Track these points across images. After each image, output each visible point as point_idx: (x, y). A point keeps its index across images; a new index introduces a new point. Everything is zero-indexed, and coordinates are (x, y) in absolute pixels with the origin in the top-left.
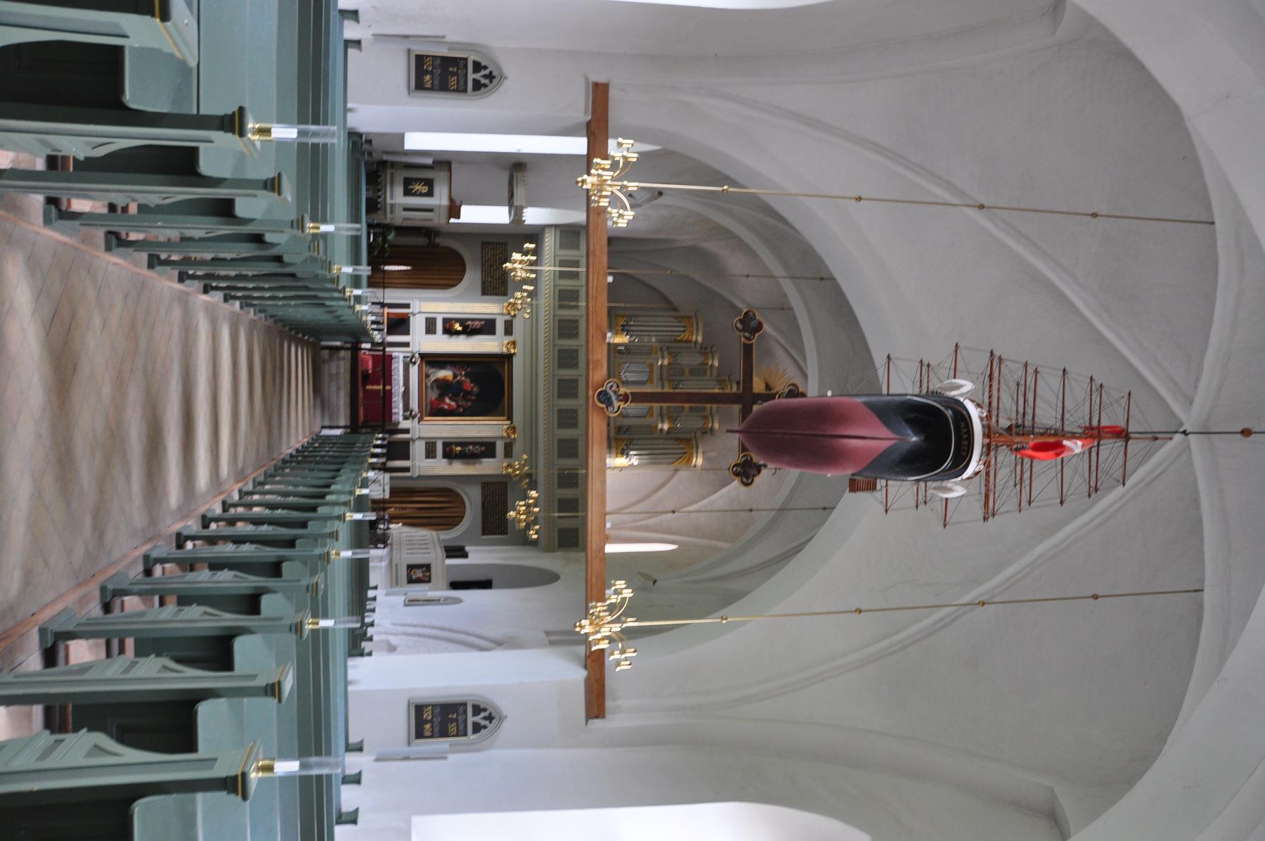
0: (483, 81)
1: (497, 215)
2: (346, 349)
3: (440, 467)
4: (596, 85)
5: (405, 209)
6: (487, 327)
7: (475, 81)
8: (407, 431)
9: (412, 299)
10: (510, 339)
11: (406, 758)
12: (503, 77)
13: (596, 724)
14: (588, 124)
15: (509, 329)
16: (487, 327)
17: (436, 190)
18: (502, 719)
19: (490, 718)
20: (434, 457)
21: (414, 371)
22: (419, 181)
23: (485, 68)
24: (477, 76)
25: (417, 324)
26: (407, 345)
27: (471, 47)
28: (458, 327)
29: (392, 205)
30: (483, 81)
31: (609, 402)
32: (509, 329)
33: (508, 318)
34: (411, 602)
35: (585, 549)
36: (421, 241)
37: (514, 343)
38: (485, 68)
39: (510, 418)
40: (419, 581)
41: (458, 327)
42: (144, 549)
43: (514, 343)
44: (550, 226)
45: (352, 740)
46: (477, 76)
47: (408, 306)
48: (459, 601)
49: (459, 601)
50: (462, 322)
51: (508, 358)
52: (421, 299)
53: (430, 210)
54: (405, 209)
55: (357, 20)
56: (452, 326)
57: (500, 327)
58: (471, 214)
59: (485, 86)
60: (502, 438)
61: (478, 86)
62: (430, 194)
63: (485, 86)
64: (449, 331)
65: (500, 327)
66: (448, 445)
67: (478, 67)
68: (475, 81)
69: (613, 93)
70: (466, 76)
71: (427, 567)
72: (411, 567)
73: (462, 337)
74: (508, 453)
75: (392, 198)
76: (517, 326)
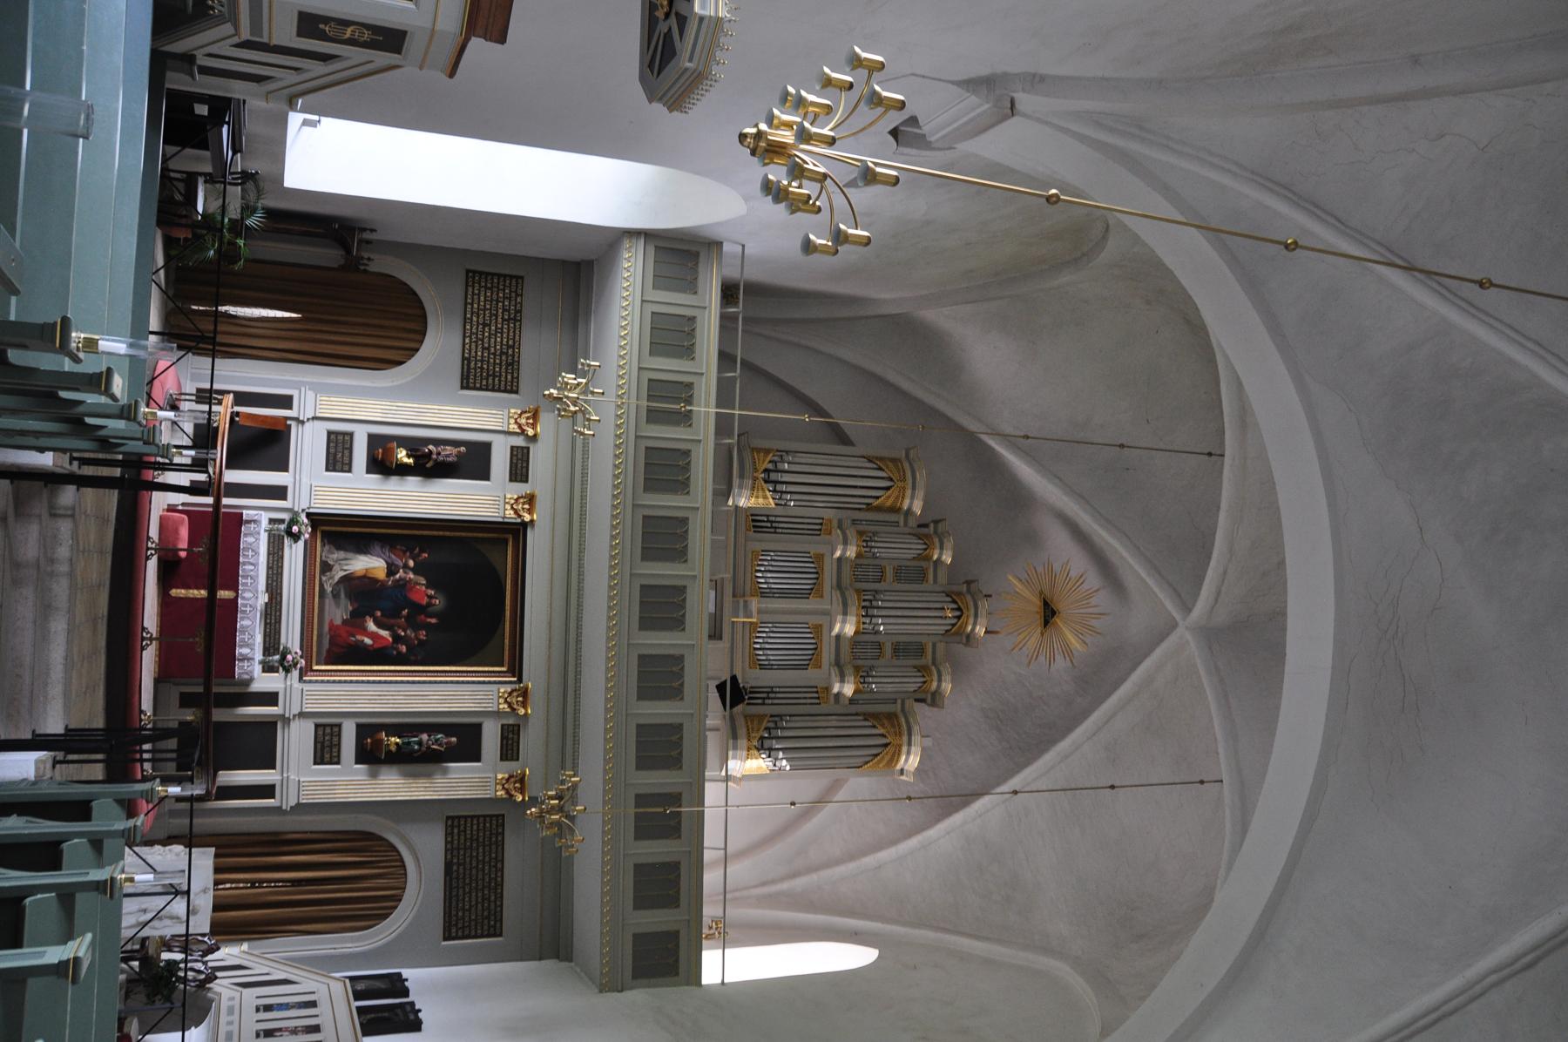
6: (470, 461)
8: (270, 698)
16: (470, 461)
20: (346, 467)
21: (294, 555)
25: (308, 445)
26: (279, 492)
33: (519, 442)
37: (531, 499)
39: (516, 669)
41: (402, 455)
43: (531, 499)
47: (286, 402)
50: (412, 445)
51: (513, 533)
52: (319, 389)
56: (389, 452)
64: (381, 464)
65: (500, 462)
66: (379, 445)
73: (413, 481)
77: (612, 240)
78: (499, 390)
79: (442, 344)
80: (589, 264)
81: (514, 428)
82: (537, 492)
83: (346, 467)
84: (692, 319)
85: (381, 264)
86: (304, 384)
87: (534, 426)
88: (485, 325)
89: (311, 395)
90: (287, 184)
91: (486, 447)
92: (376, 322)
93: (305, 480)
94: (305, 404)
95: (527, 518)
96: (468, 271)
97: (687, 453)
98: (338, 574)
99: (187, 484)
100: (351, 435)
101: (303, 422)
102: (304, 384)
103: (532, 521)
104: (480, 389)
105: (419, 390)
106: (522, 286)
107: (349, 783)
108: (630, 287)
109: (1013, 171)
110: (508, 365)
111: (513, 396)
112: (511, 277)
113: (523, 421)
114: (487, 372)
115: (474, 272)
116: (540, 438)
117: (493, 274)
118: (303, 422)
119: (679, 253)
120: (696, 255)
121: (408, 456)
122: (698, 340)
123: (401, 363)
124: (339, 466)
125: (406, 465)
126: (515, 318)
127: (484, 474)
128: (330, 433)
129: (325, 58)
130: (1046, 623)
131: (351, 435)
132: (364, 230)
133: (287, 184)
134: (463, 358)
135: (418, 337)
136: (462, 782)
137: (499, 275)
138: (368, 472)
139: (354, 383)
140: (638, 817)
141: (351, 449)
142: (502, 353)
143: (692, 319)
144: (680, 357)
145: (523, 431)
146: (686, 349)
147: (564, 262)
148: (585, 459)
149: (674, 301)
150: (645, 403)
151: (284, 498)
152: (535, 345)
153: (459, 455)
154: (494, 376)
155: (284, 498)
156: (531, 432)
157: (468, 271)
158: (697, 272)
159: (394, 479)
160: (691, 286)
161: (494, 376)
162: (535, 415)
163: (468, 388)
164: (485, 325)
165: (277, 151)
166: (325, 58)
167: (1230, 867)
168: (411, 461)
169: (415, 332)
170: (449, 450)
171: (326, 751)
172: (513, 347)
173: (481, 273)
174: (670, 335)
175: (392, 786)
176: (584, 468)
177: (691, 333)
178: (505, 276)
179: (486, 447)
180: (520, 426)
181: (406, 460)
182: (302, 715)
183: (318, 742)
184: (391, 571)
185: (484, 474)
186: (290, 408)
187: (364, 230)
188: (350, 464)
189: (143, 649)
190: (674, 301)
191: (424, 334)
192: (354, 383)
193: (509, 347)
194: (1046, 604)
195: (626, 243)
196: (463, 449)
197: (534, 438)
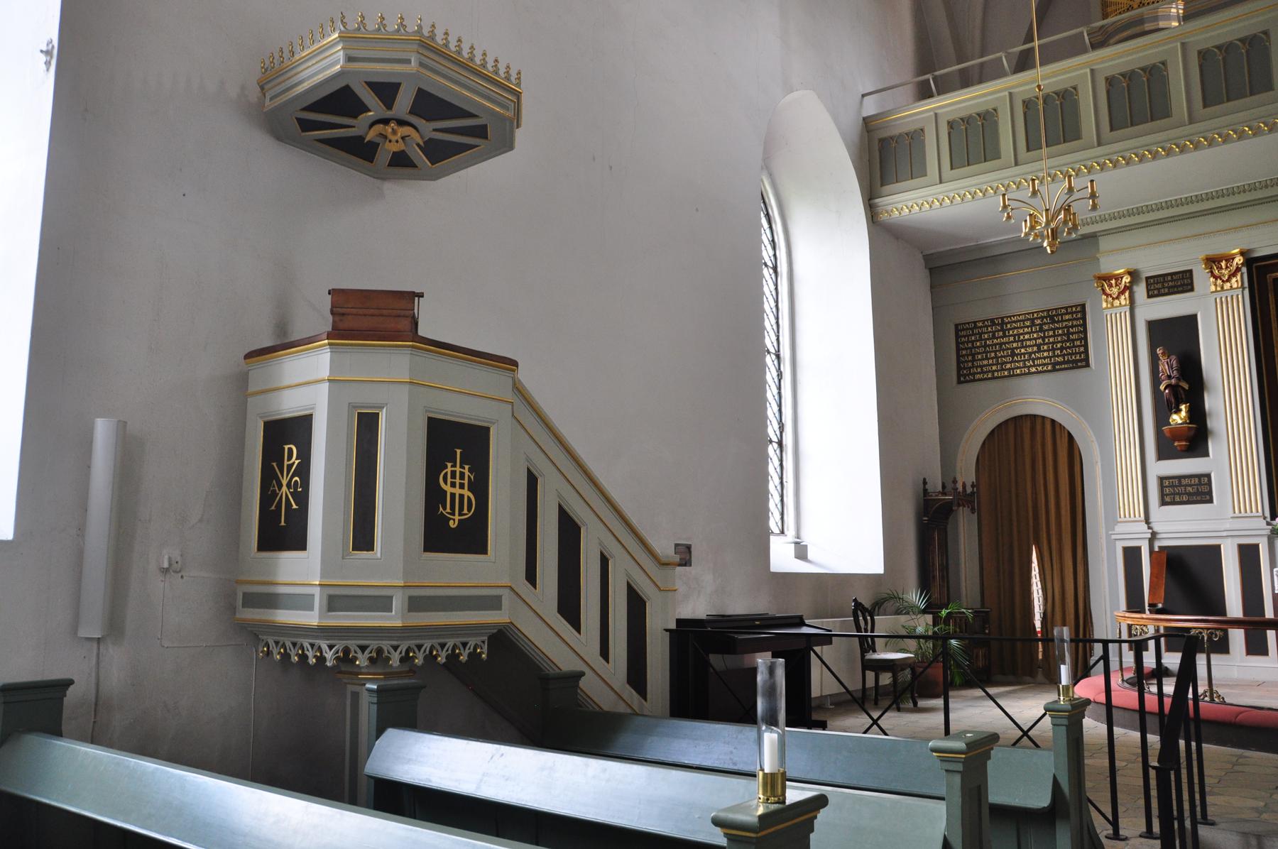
5: (363, 538)
6: (1176, 341)
9: (1111, 544)
10: (1202, 278)
15: (1181, 282)
16: (1176, 341)
25: (1182, 526)
26: (1248, 555)
28: (1178, 418)
29: (334, 603)
33: (1141, 290)
36: (966, 533)
37: (1212, 262)
41: (1178, 418)
42: (870, 108)
43: (1212, 262)
45: (664, 547)
47: (1132, 555)
50: (1163, 409)
52: (1112, 520)
53: (367, 424)
56: (1177, 434)
64: (1195, 439)
65: (1171, 307)
73: (1211, 402)
75: (303, 603)
77: (886, 237)
78: (1084, 325)
79: (1039, 396)
80: (928, 259)
81: (1124, 300)
82: (1202, 256)
84: (951, 124)
85: (966, 474)
86: (1108, 536)
87: (1118, 278)
88: (1013, 355)
89: (1119, 528)
90: (881, 571)
91: (1153, 326)
92: (1028, 467)
93: (1228, 526)
94: (1135, 534)
95: (1239, 260)
96: (959, 382)
97: (1110, 81)
99: (1132, 653)
100: (1162, 479)
101: (1154, 534)
102: (1108, 536)
103: (1242, 253)
104: (1086, 346)
105: (1098, 413)
106: (959, 321)
108: (935, 201)
110: (1053, 322)
111: (1088, 309)
112: (957, 336)
113: (1115, 291)
114: (1068, 342)
115: (959, 376)
116: (1132, 267)
117: (958, 356)
118: (1154, 534)
119: (882, 158)
120: (882, 141)
121: (1178, 411)
122: (973, 111)
123: (1070, 437)
124: (1205, 489)
125: (1190, 412)
126: (1001, 324)
127: (1189, 322)
128: (1163, 503)
129: (604, 561)
131: (1162, 479)
132: (925, 491)
133: (881, 571)
134: (1054, 370)
135: (1039, 422)
137: (958, 350)
138: (1207, 455)
139: (1100, 482)
140: (939, 94)
141: (1180, 478)
142: (1041, 330)
143: (951, 124)
144: (996, 123)
145: (1126, 288)
146: (986, 120)
147: (932, 287)
148: (1150, 209)
149: (934, 150)
150: (1045, 151)
151: (1255, 547)
152: (1025, 296)
153: (1168, 353)
154: (1069, 334)
155: (1137, 550)
156: (1127, 279)
157: (959, 382)
158: (900, 135)
159: (1210, 423)
160: (915, 137)
161: (1069, 334)
162: (1106, 278)
163: (1087, 360)
164: (1013, 355)
165: (828, 586)
166: (604, 561)
168: (1183, 407)
169: (1033, 429)
170: (1164, 366)
171: (1196, 491)
172: (1032, 320)
173: (959, 369)
174: (973, 142)
176: (1160, 207)
177: (967, 120)
178: (958, 343)
179: (1153, 326)
180: (1122, 292)
181: (1183, 414)
182: (1147, 521)
185: (1189, 322)
186: (1139, 549)
187: (925, 491)
188: (1199, 476)
189: (1224, 703)
190: (934, 150)
191: (1035, 416)
192: (1100, 482)
193: (1033, 324)
195: (884, 217)
196: (1159, 351)
197: (1134, 274)
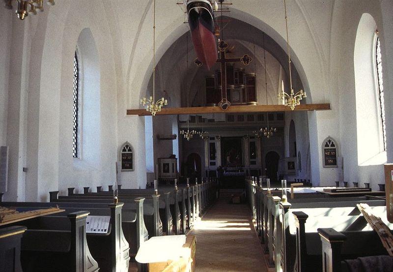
0: (128, 148)
1: (175, 143)
2: (219, 190)
3: (259, 159)
4: (127, 114)
7: (128, 151)
8: (247, 171)
11: (342, 168)
12: (127, 143)
13: (332, 105)
14: (139, 115)
15: (213, 139)
17: (166, 162)
18: (127, 143)
19: (330, 141)
20: (255, 162)
21: (228, 169)
22: (164, 168)
23: (124, 148)
24: (127, 150)
27: (119, 152)
30: (331, 143)
31: (226, 105)
32: (213, 139)
34: (300, 169)
35: (284, 112)
37: (217, 137)
38: (124, 148)
39: (242, 137)
40: (294, 166)
43: (217, 137)
44: (178, 126)
46: (127, 150)
48: (299, 152)
49: (299, 152)
51: (222, 139)
53: (173, 164)
54: (173, 172)
55: (112, 186)
57: (212, 141)
58: (176, 151)
59: (130, 148)
60: (248, 139)
61: (130, 150)
62: (168, 164)
63: (130, 148)
64: (254, 157)
65: (212, 141)
66: (252, 157)
67: (124, 150)
68: (128, 151)
69: (130, 108)
70: (127, 154)
71: (289, 163)
72: (289, 168)
74: (253, 137)
76: (211, 135)
83: (255, 162)
91: (210, 144)
98: (230, 162)
107: (259, 159)
109: (36, 153)
130: (230, 52)
136: (218, 145)
167: (153, 74)
175: (259, 153)
183: (253, 164)
184: (228, 156)
194: (230, 52)
